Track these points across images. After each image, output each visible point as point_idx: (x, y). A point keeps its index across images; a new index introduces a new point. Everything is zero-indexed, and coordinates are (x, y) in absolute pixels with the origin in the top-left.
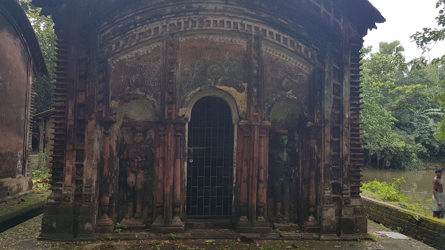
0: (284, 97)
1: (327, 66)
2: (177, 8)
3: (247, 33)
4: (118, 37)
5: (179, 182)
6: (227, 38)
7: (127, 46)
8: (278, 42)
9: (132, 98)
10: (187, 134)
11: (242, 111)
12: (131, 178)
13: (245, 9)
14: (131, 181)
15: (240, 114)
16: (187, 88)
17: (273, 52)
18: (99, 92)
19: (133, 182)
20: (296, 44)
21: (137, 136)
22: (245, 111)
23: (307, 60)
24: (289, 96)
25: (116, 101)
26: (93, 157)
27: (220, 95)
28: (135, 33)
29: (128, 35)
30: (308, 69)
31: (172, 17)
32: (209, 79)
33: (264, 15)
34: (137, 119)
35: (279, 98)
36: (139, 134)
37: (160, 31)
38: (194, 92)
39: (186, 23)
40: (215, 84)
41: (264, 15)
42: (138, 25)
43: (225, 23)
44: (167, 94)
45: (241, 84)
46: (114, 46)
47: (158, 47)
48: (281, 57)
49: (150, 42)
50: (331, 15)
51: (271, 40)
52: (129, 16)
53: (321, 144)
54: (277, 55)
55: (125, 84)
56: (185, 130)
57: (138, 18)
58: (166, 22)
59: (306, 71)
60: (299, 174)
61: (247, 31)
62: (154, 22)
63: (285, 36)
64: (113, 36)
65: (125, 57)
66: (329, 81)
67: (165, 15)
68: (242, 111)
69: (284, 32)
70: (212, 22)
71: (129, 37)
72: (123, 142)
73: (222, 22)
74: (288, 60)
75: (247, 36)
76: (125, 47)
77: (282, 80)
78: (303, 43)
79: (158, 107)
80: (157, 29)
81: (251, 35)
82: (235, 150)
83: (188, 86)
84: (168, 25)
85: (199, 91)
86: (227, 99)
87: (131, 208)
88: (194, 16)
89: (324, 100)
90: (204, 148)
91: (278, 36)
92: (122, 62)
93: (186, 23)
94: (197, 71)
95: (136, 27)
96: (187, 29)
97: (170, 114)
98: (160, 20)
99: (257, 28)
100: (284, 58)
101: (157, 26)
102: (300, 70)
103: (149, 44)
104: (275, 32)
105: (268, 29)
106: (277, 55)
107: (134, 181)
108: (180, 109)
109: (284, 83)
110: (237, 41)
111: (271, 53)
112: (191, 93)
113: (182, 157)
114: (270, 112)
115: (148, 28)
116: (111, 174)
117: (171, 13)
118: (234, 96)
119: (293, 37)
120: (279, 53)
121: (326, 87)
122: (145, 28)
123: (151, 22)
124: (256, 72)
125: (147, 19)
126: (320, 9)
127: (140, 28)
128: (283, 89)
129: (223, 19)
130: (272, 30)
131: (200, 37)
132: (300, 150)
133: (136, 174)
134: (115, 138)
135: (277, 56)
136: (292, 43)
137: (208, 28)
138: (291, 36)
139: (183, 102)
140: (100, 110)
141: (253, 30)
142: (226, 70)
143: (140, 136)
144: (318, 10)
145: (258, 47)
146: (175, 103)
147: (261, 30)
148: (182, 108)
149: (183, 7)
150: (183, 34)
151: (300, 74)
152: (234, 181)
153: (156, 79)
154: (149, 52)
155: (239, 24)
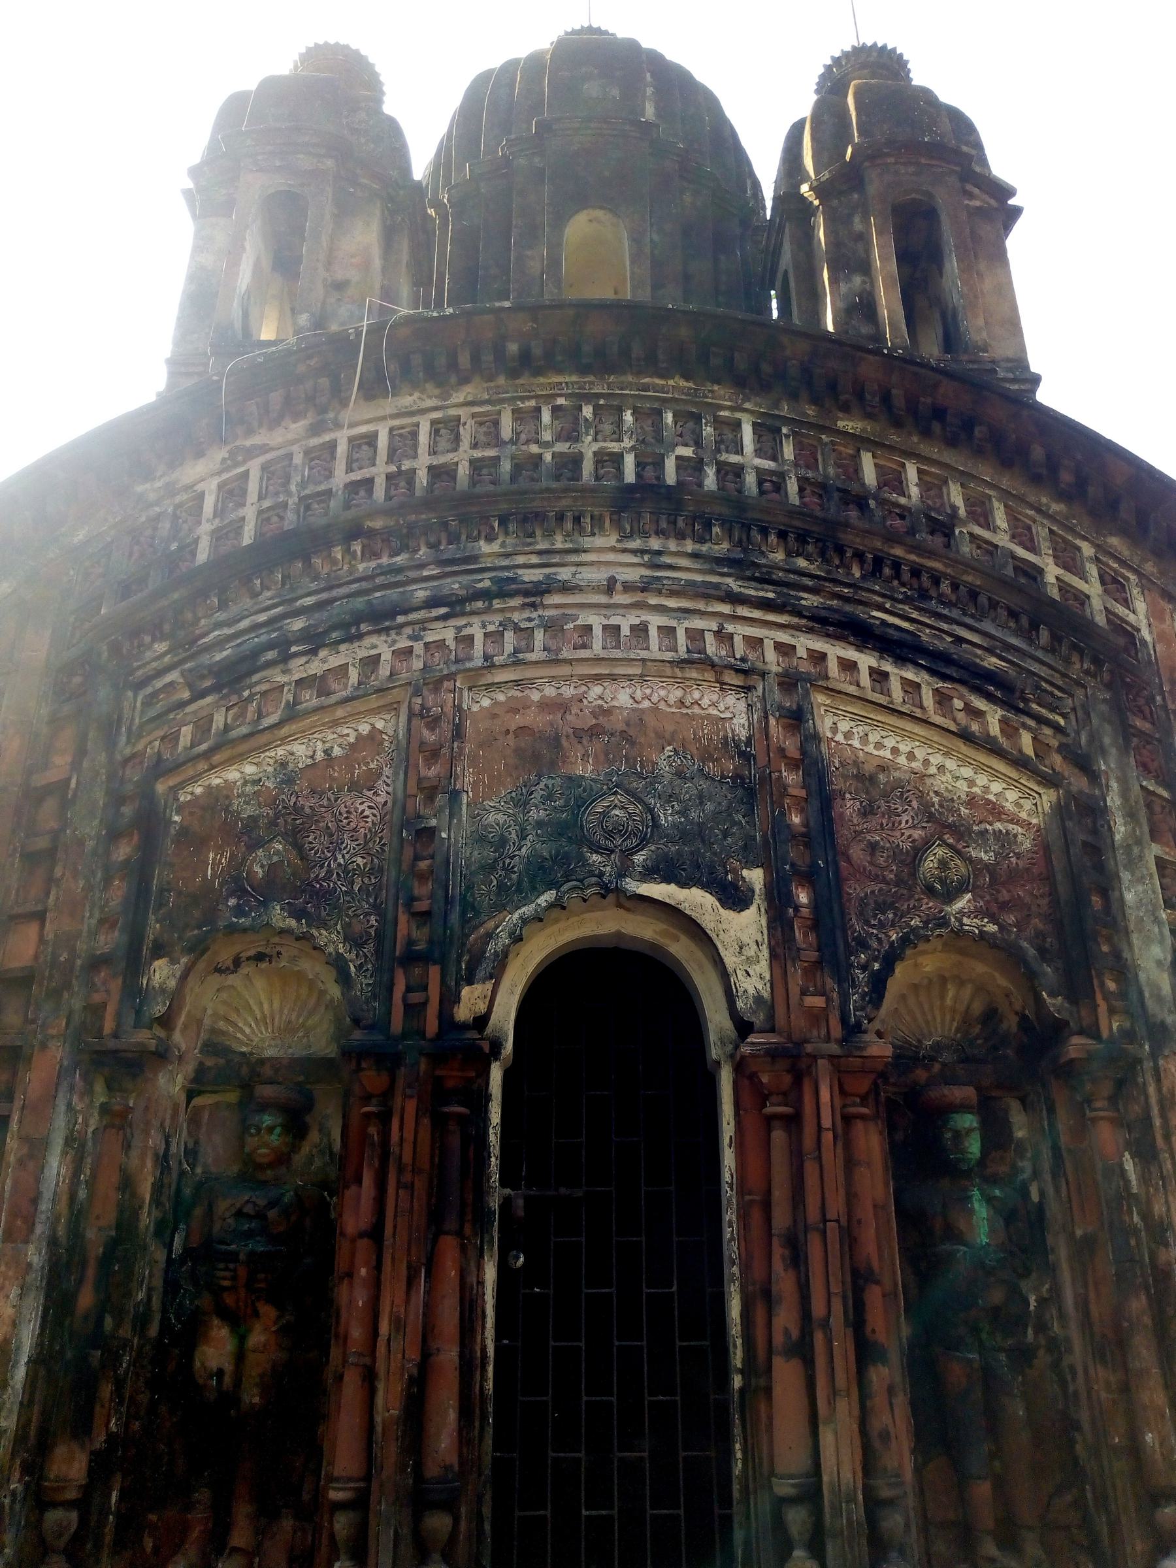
0: (939, 926)
1: (1114, 785)
2: (456, 586)
3: (745, 666)
4: (209, 699)
5: (449, 1355)
6: (663, 693)
7: (244, 730)
8: (883, 700)
9: (251, 953)
10: (495, 1117)
11: (751, 991)
12: (216, 1351)
13: (729, 581)
14: (213, 1365)
15: (740, 1004)
16: (498, 894)
17: (864, 739)
18: (101, 922)
19: (220, 1373)
20: (958, 704)
21: (259, 1130)
22: (766, 994)
23: (1020, 762)
24: (960, 921)
25: (173, 961)
26: (31, 1228)
27: (643, 929)
28: (281, 679)
29: (250, 687)
30: (1027, 804)
31: (437, 619)
32: (595, 857)
33: (810, 600)
34: (269, 1053)
35: (914, 930)
36: (267, 1120)
37: (384, 671)
38: (527, 910)
39: (495, 637)
40: (621, 875)
41: (810, 600)
42: (294, 649)
43: (653, 632)
44: (403, 918)
45: (734, 871)
46: (186, 733)
47: (374, 737)
48: (902, 760)
49: (340, 713)
50: (1093, 588)
51: (852, 689)
52: (262, 618)
53: (1153, 1145)
54: (881, 753)
55: (221, 885)
56: (488, 1098)
57: (298, 624)
58: (410, 638)
59: (1023, 815)
60: (1062, 1316)
61: (743, 660)
62: (360, 636)
63: (910, 674)
64: (186, 695)
65: (233, 775)
66: (1136, 850)
67: (405, 612)
68: (751, 991)
69: (901, 660)
70: (597, 631)
71: (252, 695)
72: (193, 1166)
73: (640, 630)
74: (933, 770)
75: (746, 675)
76: (234, 734)
77: (919, 851)
78: (990, 697)
79: (363, 983)
80: (373, 662)
81: (763, 675)
82: (728, 1193)
83: (501, 886)
84: (418, 648)
85: (551, 906)
86: (681, 949)
87: (199, 1518)
88: (526, 614)
89: (1127, 933)
90: (579, 1193)
91: (879, 677)
92: (217, 800)
93: (495, 637)
94: (540, 824)
95: (285, 658)
96: (497, 660)
97: (414, 1010)
98: (387, 630)
99: (784, 649)
100: (914, 765)
101: (373, 652)
102: (996, 811)
103: (336, 723)
104: (866, 660)
105: (835, 651)
106: (881, 753)
107: (228, 1367)
108: (465, 991)
109: (930, 864)
110: (705, 702)
111: (856, 743)
112: (516, 916)
113: (468, 1230)
114: (881, 997)
115: (334, 661)
116: (118, 1325)
117: (431, 603)
118: (708, 923)
119: (944, 677)
120: (890, 743)
121: (1126, 876)
122: (324, 661)
123: (350, 639)
124: (796, 819)
125: (334, 628)
126: (1041, 571)
127: (303, 660)
128: (930, 891)
129: (643, 618)
130: (851, 654)
131: (550, 691)
132: (1050, 1191)
133: (237, 1322)
134: (155, 1140)
135: (887, 754)
136: (943, 700)
137: (583, 654)
138: (932, 672)
139: (476, 960)
140: (97, 998)
141: (771, 655)
142: (667, 817)
143: (270, 1130)
144: (1034, 574)
145: (797, 718)
146: (443, 962)
147: (802, 652)
148: (470, 982)
149: (481, 580)
150: (476, 680)
151: (998, 826)
152: (737, 1359)
153: (360, 861)
154: (337, 751)
155: (709, 638)
